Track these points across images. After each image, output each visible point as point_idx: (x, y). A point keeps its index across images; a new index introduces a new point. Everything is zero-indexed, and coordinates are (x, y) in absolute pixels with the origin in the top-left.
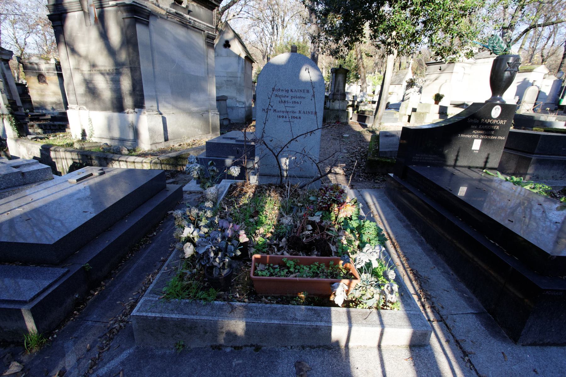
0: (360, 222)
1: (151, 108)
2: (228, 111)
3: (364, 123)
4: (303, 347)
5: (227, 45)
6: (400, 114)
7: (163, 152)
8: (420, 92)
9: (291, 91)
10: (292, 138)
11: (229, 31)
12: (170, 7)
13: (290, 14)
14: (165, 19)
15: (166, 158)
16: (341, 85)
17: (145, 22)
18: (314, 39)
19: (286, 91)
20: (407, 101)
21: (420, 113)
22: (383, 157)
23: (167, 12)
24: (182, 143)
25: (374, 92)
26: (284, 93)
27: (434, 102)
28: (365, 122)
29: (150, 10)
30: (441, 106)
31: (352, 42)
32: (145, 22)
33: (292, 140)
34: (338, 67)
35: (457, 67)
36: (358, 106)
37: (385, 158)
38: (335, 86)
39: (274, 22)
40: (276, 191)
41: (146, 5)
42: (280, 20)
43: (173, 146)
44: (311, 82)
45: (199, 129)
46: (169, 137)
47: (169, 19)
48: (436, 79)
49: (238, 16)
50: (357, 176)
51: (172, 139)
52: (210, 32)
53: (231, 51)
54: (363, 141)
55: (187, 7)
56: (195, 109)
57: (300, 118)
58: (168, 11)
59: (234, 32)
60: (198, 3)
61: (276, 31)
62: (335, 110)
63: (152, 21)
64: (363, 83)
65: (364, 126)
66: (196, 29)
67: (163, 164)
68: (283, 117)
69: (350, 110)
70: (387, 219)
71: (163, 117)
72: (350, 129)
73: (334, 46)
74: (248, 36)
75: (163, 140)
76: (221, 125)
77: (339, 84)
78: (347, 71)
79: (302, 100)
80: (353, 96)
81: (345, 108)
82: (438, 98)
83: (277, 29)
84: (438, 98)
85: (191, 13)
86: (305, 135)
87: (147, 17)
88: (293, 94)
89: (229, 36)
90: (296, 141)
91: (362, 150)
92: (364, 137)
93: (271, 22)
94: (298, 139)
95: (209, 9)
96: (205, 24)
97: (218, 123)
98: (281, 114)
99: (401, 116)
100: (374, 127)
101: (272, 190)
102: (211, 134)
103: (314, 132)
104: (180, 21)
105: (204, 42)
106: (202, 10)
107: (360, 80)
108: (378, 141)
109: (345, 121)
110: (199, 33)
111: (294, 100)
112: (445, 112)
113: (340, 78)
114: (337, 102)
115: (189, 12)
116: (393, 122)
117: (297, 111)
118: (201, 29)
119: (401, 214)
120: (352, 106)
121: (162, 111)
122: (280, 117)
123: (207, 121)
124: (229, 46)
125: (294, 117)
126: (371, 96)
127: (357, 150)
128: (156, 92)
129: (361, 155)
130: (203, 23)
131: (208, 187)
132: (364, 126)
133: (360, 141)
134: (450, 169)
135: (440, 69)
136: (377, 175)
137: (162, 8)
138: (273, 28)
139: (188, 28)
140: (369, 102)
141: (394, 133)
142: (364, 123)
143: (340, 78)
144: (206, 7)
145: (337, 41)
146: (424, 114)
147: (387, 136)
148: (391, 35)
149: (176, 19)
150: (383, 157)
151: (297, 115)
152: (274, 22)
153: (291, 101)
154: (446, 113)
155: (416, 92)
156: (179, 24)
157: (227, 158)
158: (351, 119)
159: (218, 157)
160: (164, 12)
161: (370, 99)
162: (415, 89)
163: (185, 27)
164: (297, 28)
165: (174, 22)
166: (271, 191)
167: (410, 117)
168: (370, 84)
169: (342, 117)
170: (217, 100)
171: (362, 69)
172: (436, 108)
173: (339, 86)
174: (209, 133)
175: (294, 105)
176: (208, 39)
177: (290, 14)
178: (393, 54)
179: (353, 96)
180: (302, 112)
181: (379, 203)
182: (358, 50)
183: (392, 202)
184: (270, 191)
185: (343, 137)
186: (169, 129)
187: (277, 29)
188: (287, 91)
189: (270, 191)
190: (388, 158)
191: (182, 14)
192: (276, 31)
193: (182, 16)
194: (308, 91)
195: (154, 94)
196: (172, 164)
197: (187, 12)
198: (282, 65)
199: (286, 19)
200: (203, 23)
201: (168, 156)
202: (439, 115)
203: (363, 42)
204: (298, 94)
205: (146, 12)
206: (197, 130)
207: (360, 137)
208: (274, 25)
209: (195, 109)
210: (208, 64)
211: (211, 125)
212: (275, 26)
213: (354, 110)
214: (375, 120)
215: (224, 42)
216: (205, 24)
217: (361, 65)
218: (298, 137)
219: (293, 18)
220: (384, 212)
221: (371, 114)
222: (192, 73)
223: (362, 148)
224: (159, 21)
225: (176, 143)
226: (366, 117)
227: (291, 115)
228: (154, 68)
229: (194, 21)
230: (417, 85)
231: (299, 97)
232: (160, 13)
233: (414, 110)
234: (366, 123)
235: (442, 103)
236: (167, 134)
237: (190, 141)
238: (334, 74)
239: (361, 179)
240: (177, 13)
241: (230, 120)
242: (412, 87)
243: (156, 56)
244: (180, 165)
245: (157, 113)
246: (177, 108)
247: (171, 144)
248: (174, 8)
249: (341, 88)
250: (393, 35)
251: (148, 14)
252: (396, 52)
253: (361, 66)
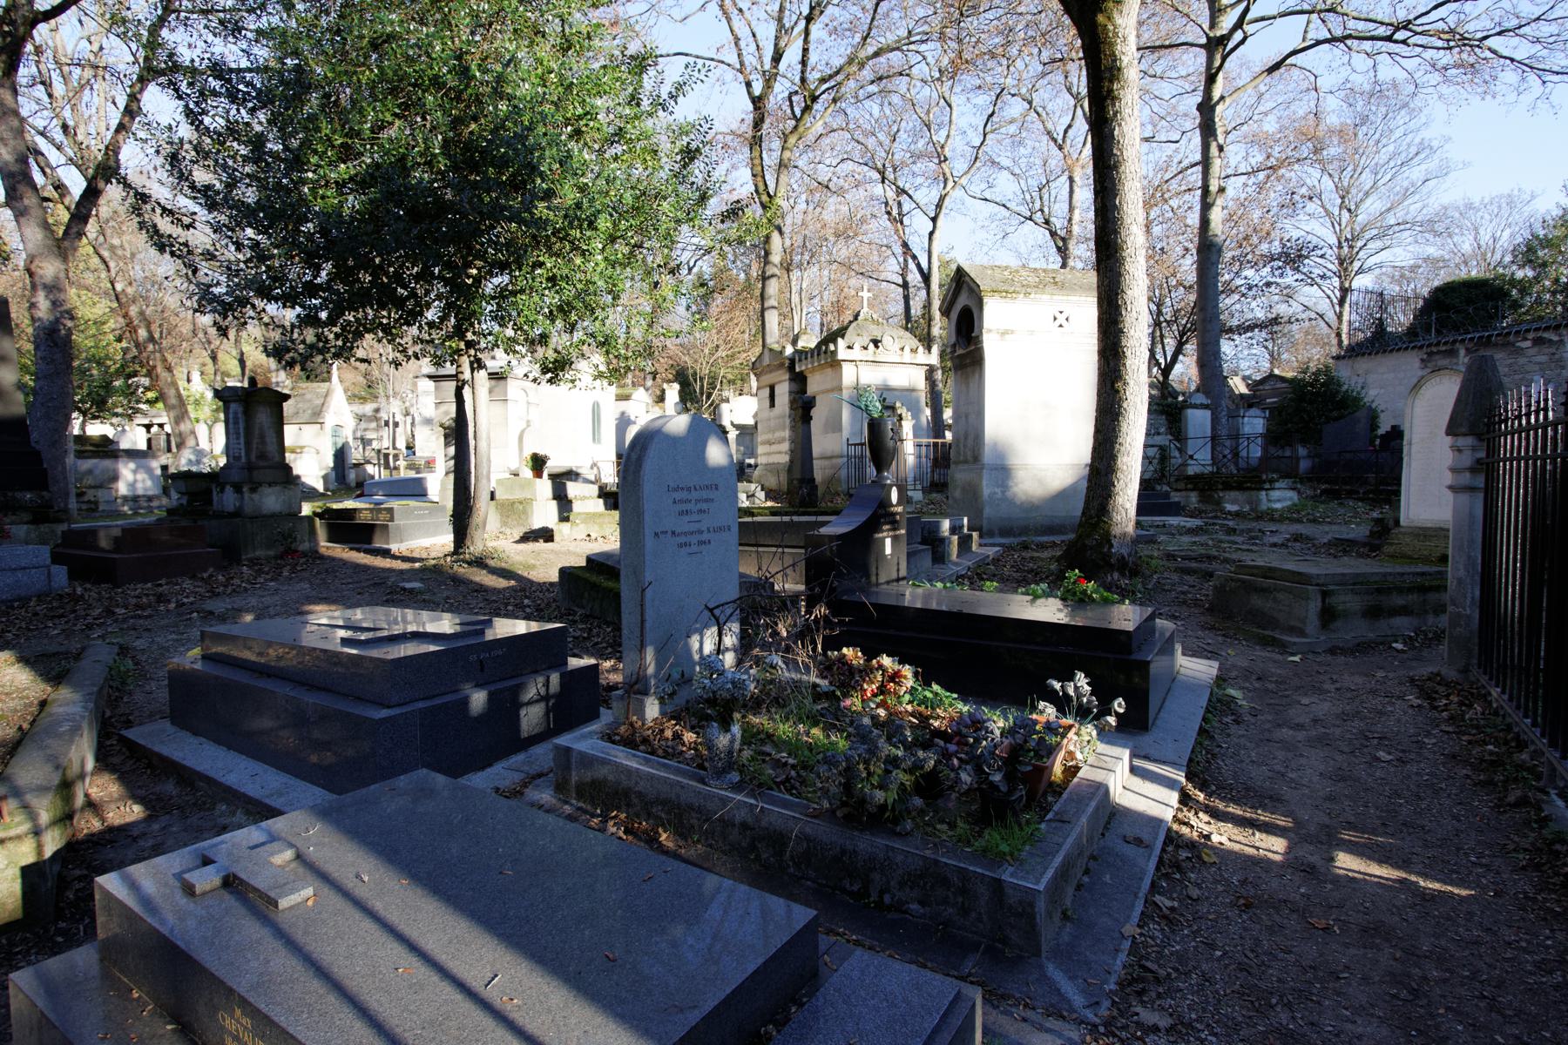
4: (1103, 835)
16: (268, 440)
38: (248, 443)
62: (264, 516)
68: (686, 544)
77: (262, 437)
82: (538, 463)
111: (699, 506)
113: (263, 417)
114: (266, 490)
117: (704, 528)
134: (874, 589)
151: (705, 537)
153: (695, 509)
154: (566, 496)
188: (689, 489)
227: (694, 539)
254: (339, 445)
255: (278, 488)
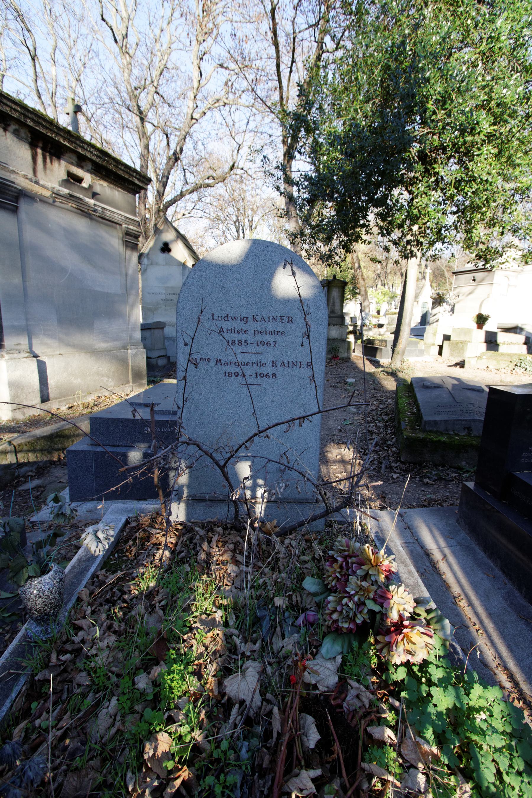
0: (449, 673)
1: (16, 347)
2: (167, 344)
3: (373, 359)
5: (166, 248)
6: (425, 344)
7: (35, 422)
8: (452, 310)
9: (254, 319)
10: (256, 431)
11: (170, 230)
12: (60, 186)
13: (260, 212)
14: (50, 204)
15: (28, 440)
16: (336, 304)
17: (10, 207)
18: (293, 237)
19: (242, 319)
20: (435, 324)
21: (457, 343)
22: (431, 431)
23: (53, 193)
24: (75, 404)
25: (378, 312)
26: (237, 326)
27: (475, 325)
28: (375, 356)
29: (20, 188)
30: (487, 333)
31: (350, 241)
32: (10, 207)
33: (255, 435)
34: (332, 278)
35: (498, 275)
36: (361, 334)
37: (436, 432)
39: (239, 223)
40: (225, 543)
41: (13, 180)
42: (247, 220)
43: (58, 409)
44: (301, 300)
45: (108, 376)
46: (51, 395)
47: (57, 204)
48: (470, 293)
49: (190, 215)
50: (386, 467)
51: (53, 399)
52: (131, 227)
53: (173, 258)
54: (380, 390)
55: (90, 187)
56: (103, 345)
57: (274, 375)
58: (55, 191)
59: (176, 230)
60: (110, 183)
61: (241, 235)
63: (24, 206)
64: (364, 301)
65: (377, 364)
66: (112, 223)
67: (21, 451)
69: (351, 338)
70: (491, 615)
71: (38, 361)
72: (354, 367)
73: (324, 249)
74: (204, 242)
75: (38, 400)
76: (151, 366)
77: (334, 303)
78: (344, 284)
79: (278, 338)
80: (351, 318)
81: (344, 337)
82: (481, 320)
83: (243, 232)
84: (481, 320)
85: (98, 196)
86: (285, 426)
87: (14, 200)
88: (258, 326)
89: (169, 236)
90: (267, 436)
91: (381, 406)
92: (379, 383)
93: (235, 223)
94: (269, 432)
95: (129, 192)
96: (122, 213)
97: (143, 364)
98: (234, 369)
99: (428, 346)
100: (394, 366)
101: (215, 538)
102: (131, 384)
103: (310, 418)
104: (77, 209)
105: (121, 242)
106: (117, 193)
107: (359, 296)
108: (415, 400)
109: (345, 355)
110: (112, 226)
111: (259, 338)
112: (493, 340)
113: (335, 293)
115: (94, 195)
116: (418, 356)
118: (115, 221)
119: (517, 593)
120: (354, 332)
121: (37, 350)
122: (230, 375)
123: (123, 362)
124: (169, 250)
125: (262, 375)
126: (375, 317)
127: (374, 407)
128: (27, 319)
129: (383, 419)
130: (119, 212)
131: (30, 577)
132: (377, 364)
133: (375, 389)
135: (474, 280)
136: (425, 467)
137: (43, 186)
138: (238, 231)
139: (91, 219)
140: (375, 325)
141: (438, 381)
142: (373, 359)
143: (335, 293)
144: (124, 190)
145: (328, 239)
146: (464, 343)
147: (427, 387)
148: (411, 230)
149: (71, 205)
150: (431, 431)
151: (268, 369)
152: (239, 223)
153: (254, 340)
154: (496, 341)
155: (447, 312)
156: (75, 213)
157: (131, 447)
158: (354, 352)
159: (114, 446)
160: (47, 194)
161: (375, 321)
162: (445, 307)
163: (87, 217)
164: (271, 230)
165: (67, 210)
166: (214, 543)
167: (441, 347)
168: (374, 301)
169: (341, 350)
170: (141, 329)
171: (361, 281)
172: (481, 335)
173: (334, 305)
174: (128, 382)
175: (261, 349)
176: (128, 237)
177: (260, 212)
178: (416, 258)
179: (351, 318)
180: (279, 364)
181: (454, 553)
182: (354, 257)
183: (485, 552)
184: (209, 542)
185: (346, 383)
186: (51, 382)
187: (243, 232)
188: (245, 320)
189: (209, 542)
190: (442, 434)
191: (81, 196)
192: (241, 235)
193: (81, 199)
194: (290, 320)
195: (24, 323)
196: (41, 450)
197: (91, 195)
198: (233, 266)
199: (256, 219)
200: (119, 212)
201: (33, 436)
202: (485, 344)
203: (367, 242)
204: (269, 326)
205: (12, 191)
206: (106, 379)
207: (374, 382)
208: (239, 227)
209: (103, 345)
210: (126, 275)
211: (130, 368)
212: (241, 228)
213: (356, 339)
214: (395, 355)
215: (161, 245)
216: (122, 213)
217: (359, 277)
218: (269, 428)
219: (265, 217)
220: (475, 586)
221: (383, 344)
222: (98, 289)
223: (381, 402)
224: (39, 206)
225: (64, 403)
226: (376, 349)
228: (24, 281)
229: (103, 208)
230: (447, 302)
231: (271, 333)
232: (41, 195)
233: (447, 338)
234: (378, 358)
235: (489, 326)
236: (48, 389)
237: (90, 399)
238: (326, 288)
239: (395, 476)
240: (71, 196)
241: (169, 358)
242: (440, 305)
243: (30, 261)
244: (58, 450)
245: (27, 354)
246: (68, 345)
247: (53, 406)
248: (66, 188)
249: (337, 308)
250: (414, 230)
251: (16, 194)
252: (419, 254)
253: (360, 277)
254: (425, 312)
255: (337, 327)
